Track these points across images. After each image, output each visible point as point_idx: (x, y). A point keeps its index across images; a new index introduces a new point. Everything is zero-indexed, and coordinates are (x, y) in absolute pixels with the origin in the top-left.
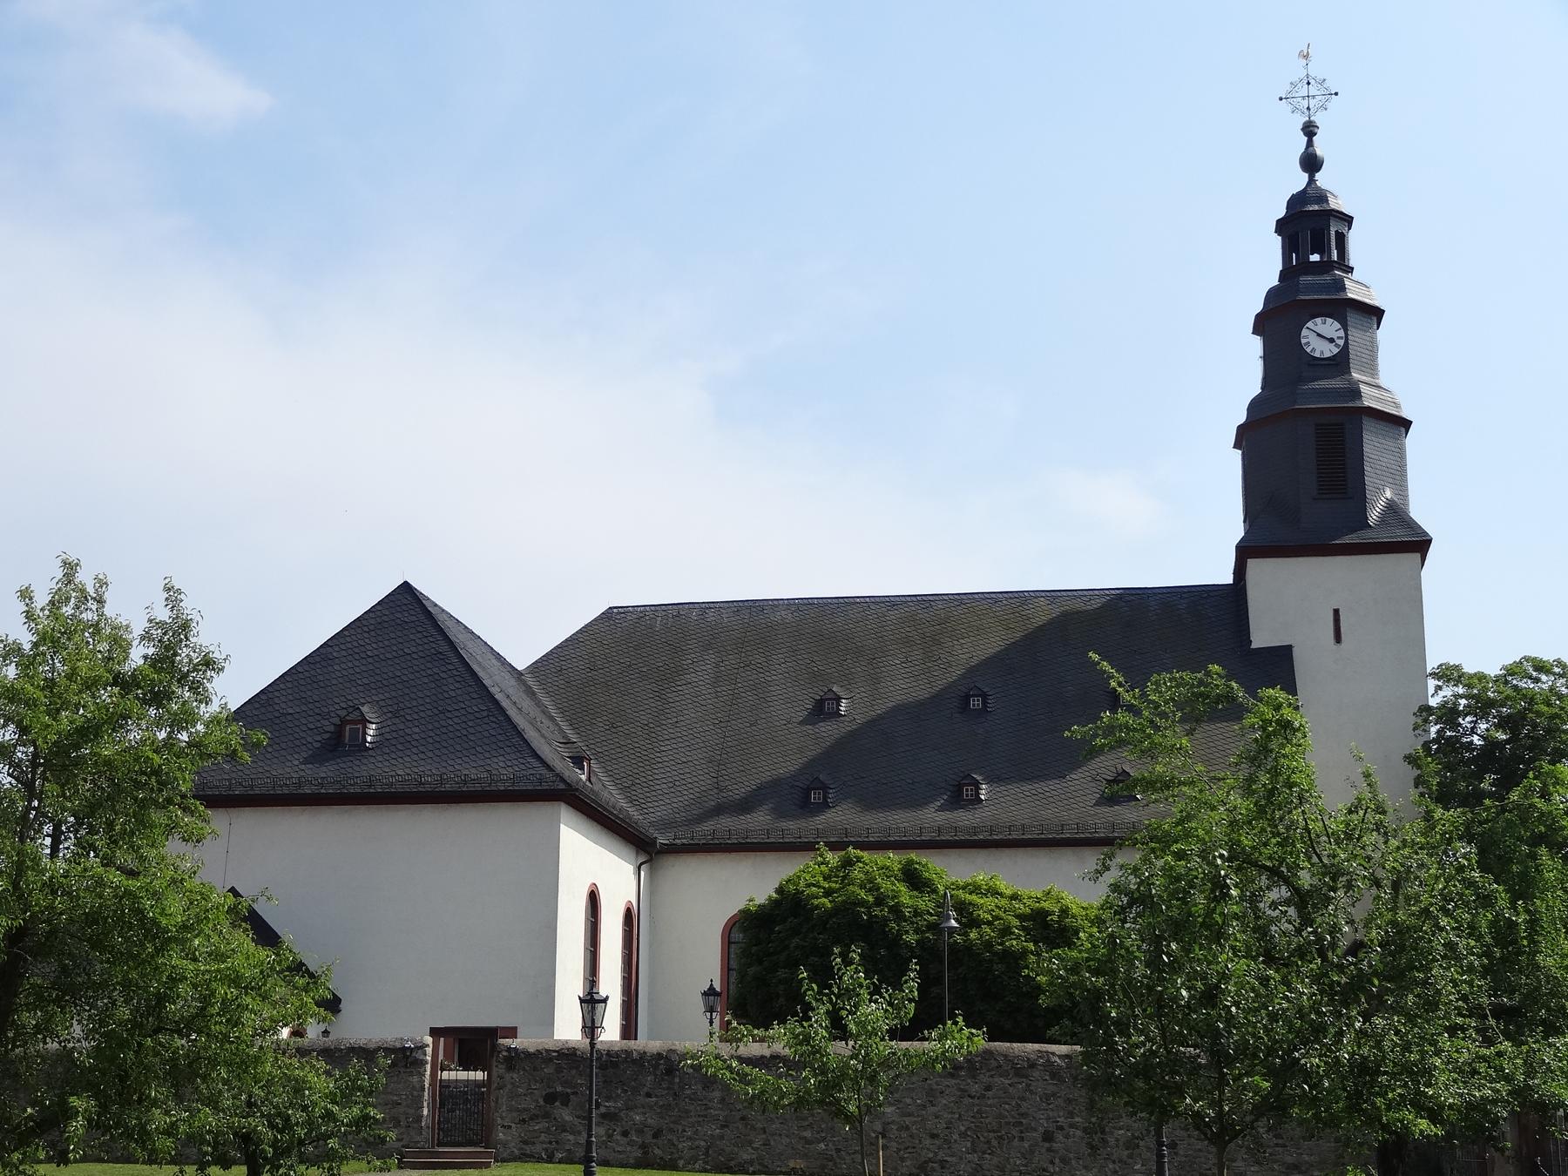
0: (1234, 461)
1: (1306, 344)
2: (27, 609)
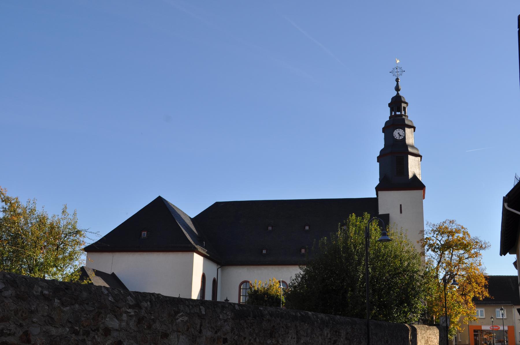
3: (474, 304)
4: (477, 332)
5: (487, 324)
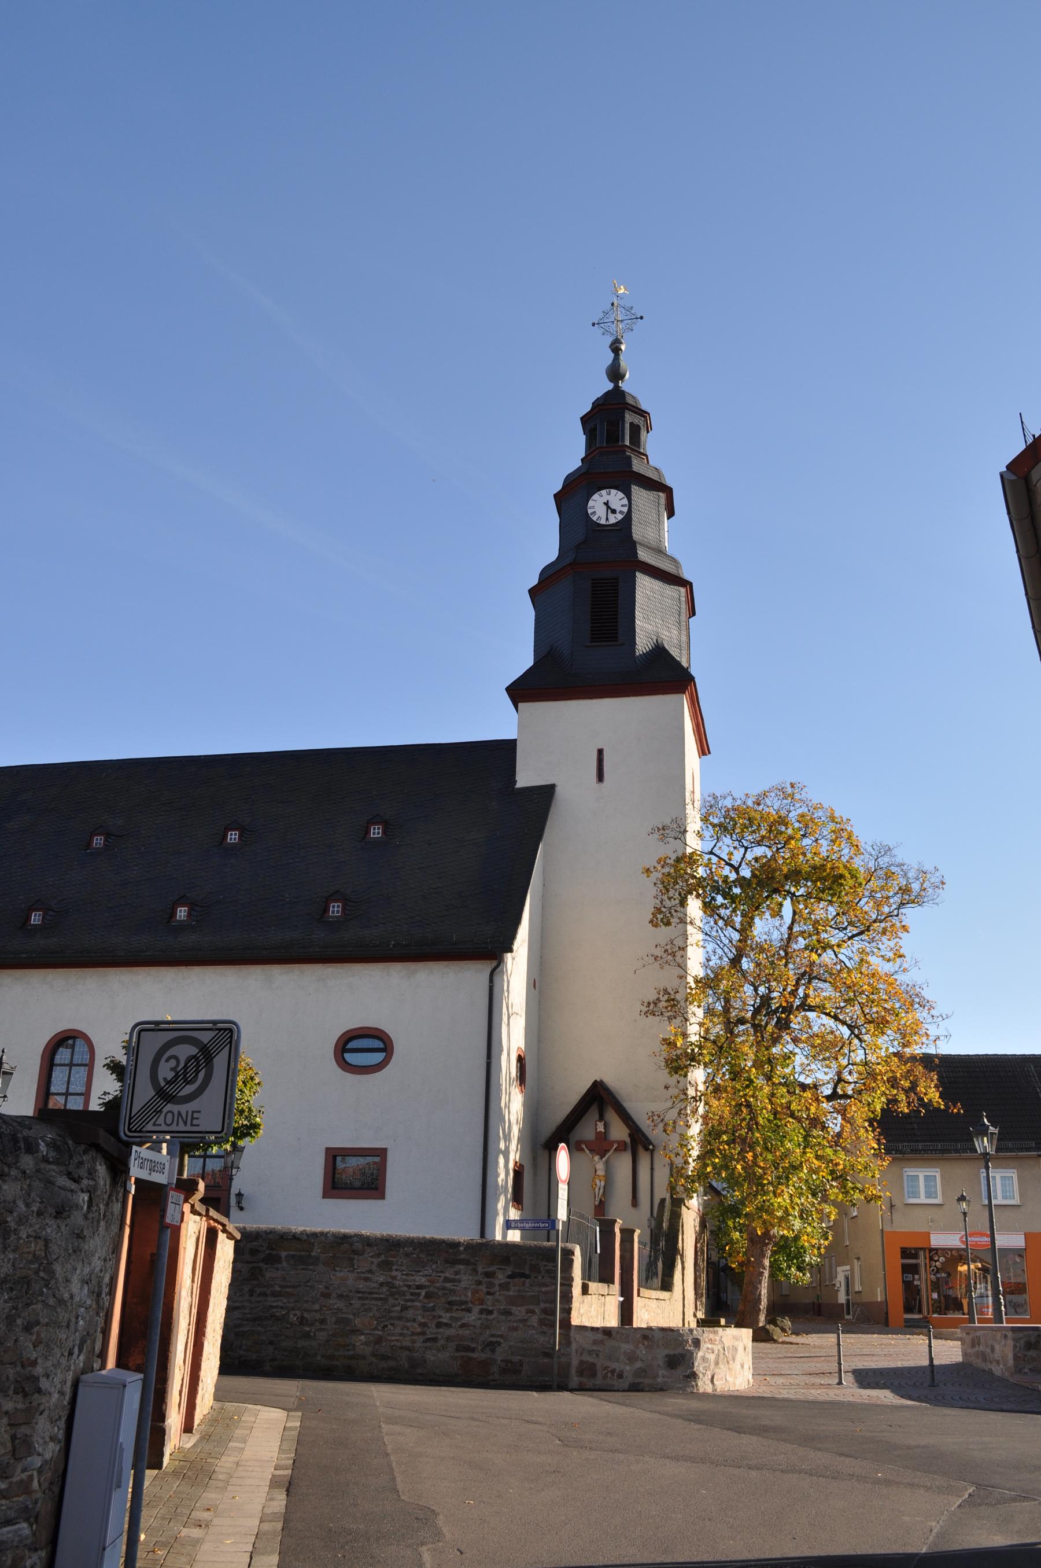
0: (527, 614)
1: (592, 514)
2: (844, 820)
3: (880, 1134)
4: (915, 1256)
5: (948, 1228)
